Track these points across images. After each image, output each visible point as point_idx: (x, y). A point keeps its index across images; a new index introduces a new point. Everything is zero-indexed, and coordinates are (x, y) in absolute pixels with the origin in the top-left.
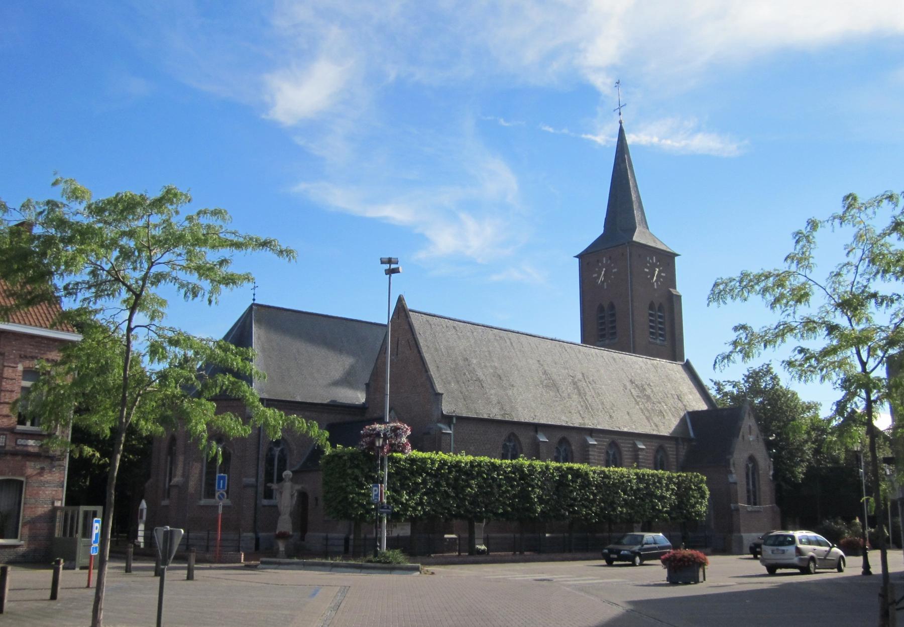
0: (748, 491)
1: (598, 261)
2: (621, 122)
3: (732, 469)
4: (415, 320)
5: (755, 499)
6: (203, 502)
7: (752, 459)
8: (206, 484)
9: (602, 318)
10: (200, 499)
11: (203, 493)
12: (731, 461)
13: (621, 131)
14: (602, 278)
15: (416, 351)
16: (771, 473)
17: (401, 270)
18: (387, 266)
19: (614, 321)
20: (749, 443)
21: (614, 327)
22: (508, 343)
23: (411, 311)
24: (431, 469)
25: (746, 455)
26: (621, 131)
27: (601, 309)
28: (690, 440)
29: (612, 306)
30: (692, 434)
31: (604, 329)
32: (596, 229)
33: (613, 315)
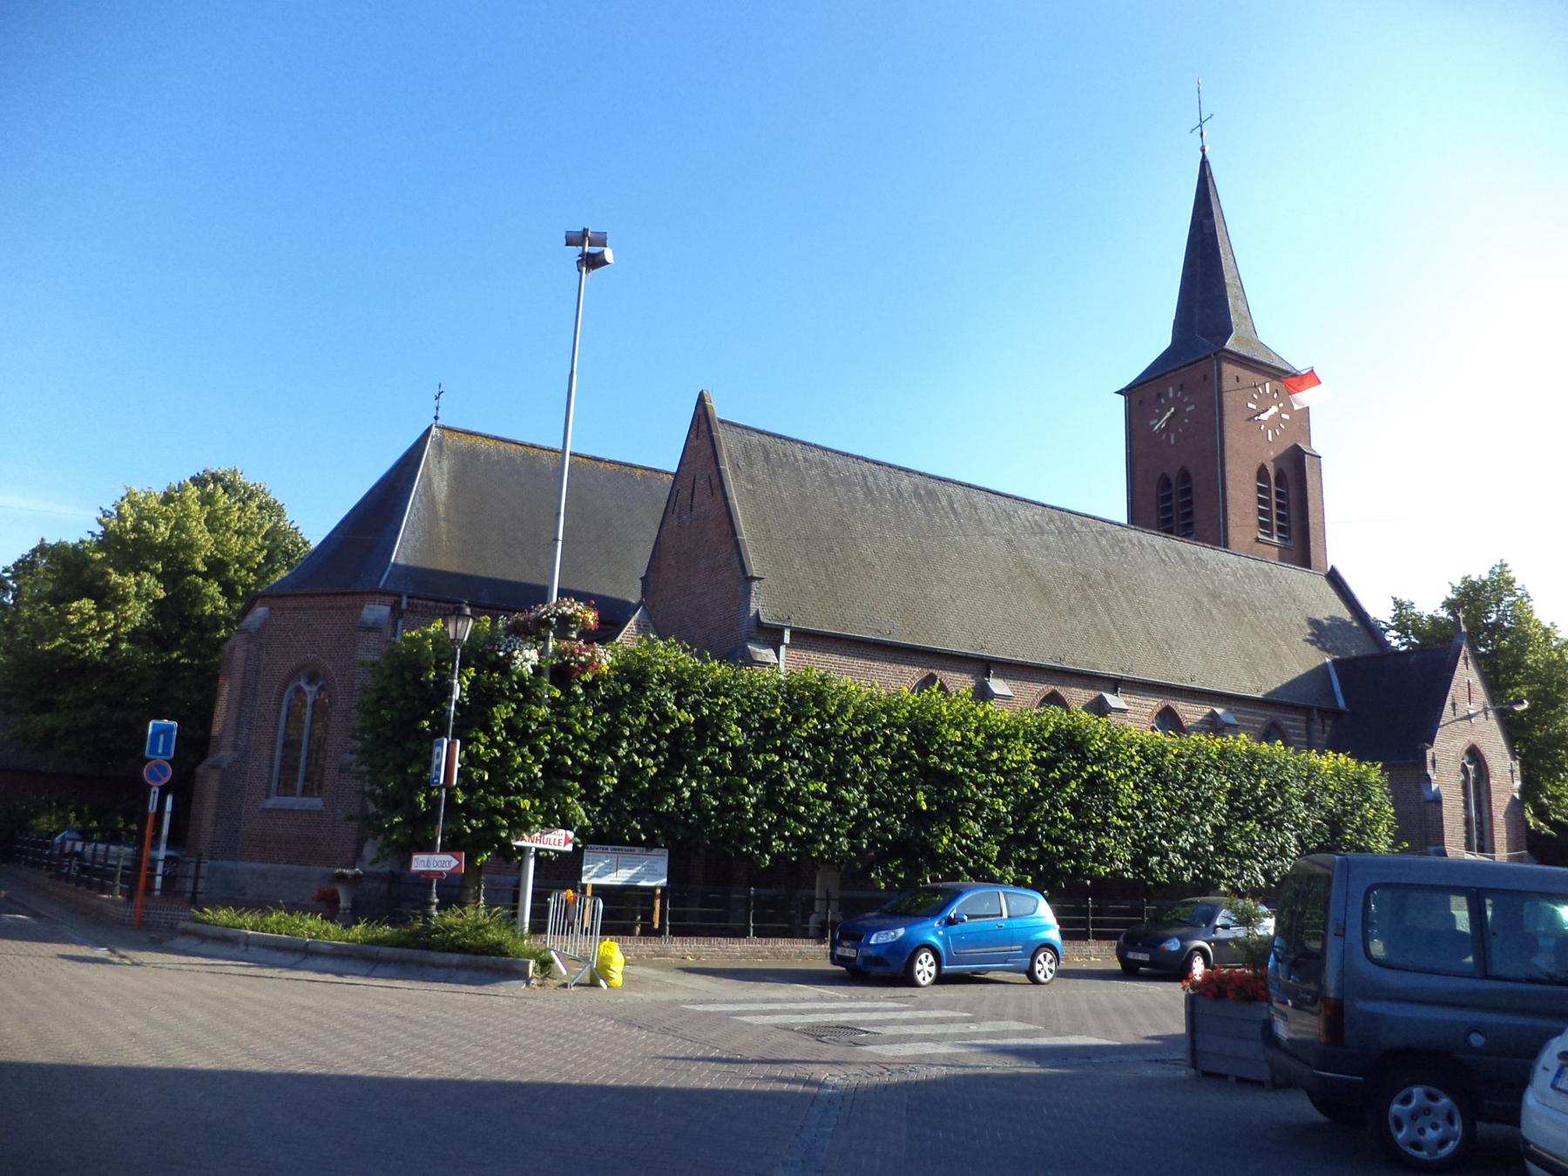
0: (1468, 822)
1: (1159, 396)
2: (1203, 150)
3: (1430, 771)
4: (721, 434)
5: (1481, 838)
6: (272, 802)
7: (1474, 754)
8: (283, 766)
9: (1169, 498)
10: (267, 797)
11: (274, 783)
12: (1429, 753)
13: (1204, 163)
14: (1162, 424)
15: (720, 498)
16: (1518, 784)
17: (609, 255)
18: (577, 250)
19: (1189, 503)
20: (1467, 724)
21: (1189, 514)
22: (944, 503)
23: (722, 422)
24: (1417, 1146)
25: (1462, 744)
26: (1204, 163)
27: (1165, 482)
28: (1337, 714)
29: (1185, 476)
30: (1342, 703)
31: (1169, 509)
32: (1155, 337)
33: (1188, 491)
